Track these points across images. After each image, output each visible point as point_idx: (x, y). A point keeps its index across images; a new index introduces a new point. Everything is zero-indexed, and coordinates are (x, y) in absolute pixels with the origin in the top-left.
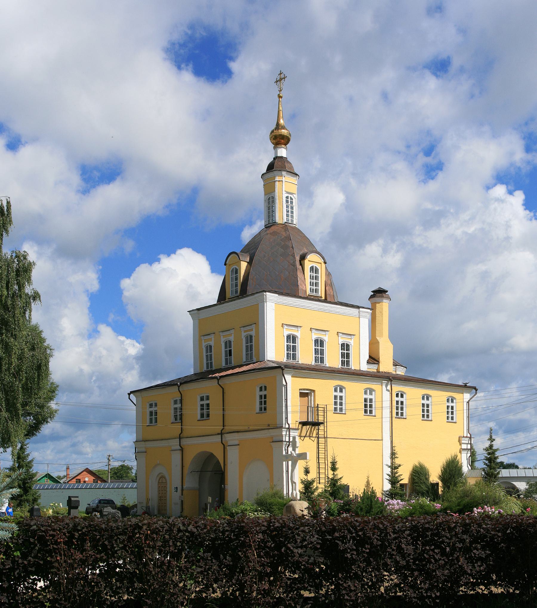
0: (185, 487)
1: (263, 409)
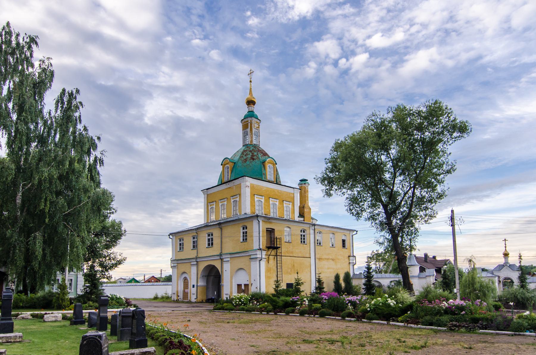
0: (198, 284)
1: (245, 240)
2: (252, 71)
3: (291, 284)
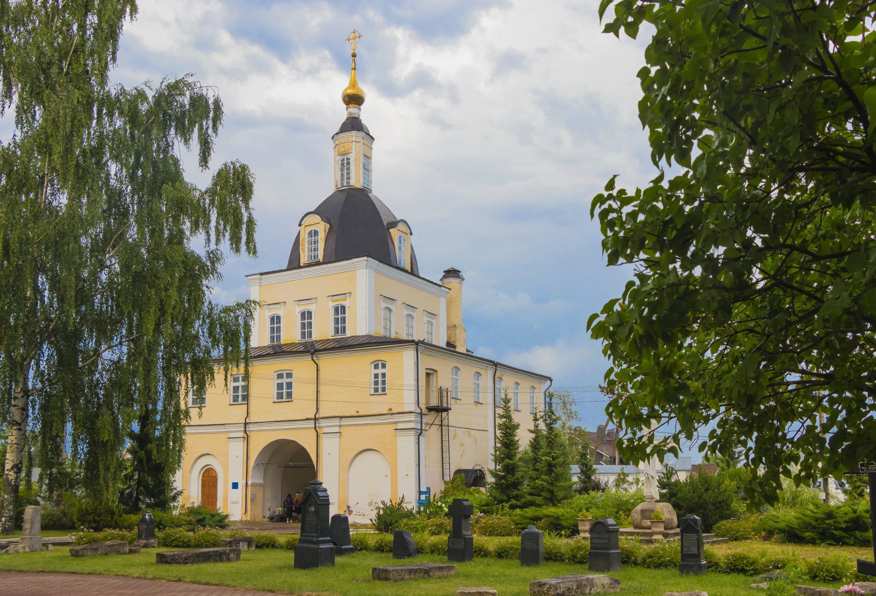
0: (249, 482)
2: (357, 34)
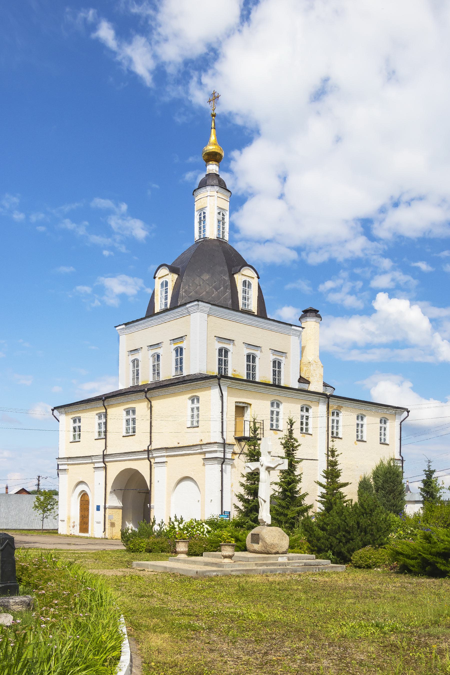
3: (88, 530)
